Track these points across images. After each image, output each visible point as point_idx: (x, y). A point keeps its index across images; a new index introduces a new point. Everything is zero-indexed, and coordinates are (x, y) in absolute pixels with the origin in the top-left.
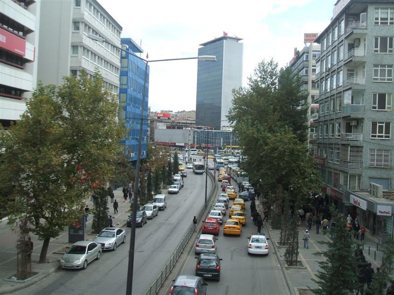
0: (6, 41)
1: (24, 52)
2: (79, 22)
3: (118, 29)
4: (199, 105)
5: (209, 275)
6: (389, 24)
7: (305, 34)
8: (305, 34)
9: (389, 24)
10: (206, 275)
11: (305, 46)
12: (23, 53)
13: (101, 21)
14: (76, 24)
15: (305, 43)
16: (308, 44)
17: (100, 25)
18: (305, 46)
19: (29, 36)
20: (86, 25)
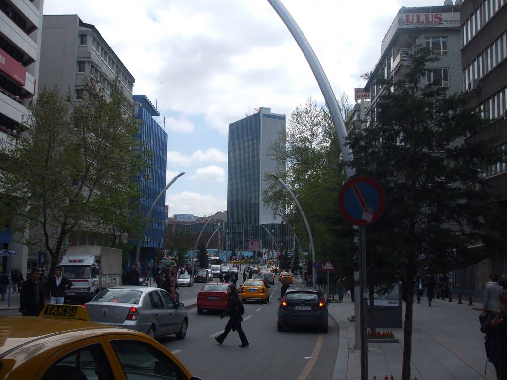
0: (5, 62)
1: (25, 80)
2: (84, 63)
3: (131, 81)
4: (230, 204)
5: (72, 294)
6: (442, 54)
7: (355, 89)
8: (355, 89)
9: (442, 54)
10: (69, 294)
11: (355, 103)
12: (23, 82)
13: (109, 65)
14: (81, 64)
15: (356, 100)
16: (360, 101)
17: (109, 70)
18: (355, 103)
19: (30, 66)
20: (93, 66)
